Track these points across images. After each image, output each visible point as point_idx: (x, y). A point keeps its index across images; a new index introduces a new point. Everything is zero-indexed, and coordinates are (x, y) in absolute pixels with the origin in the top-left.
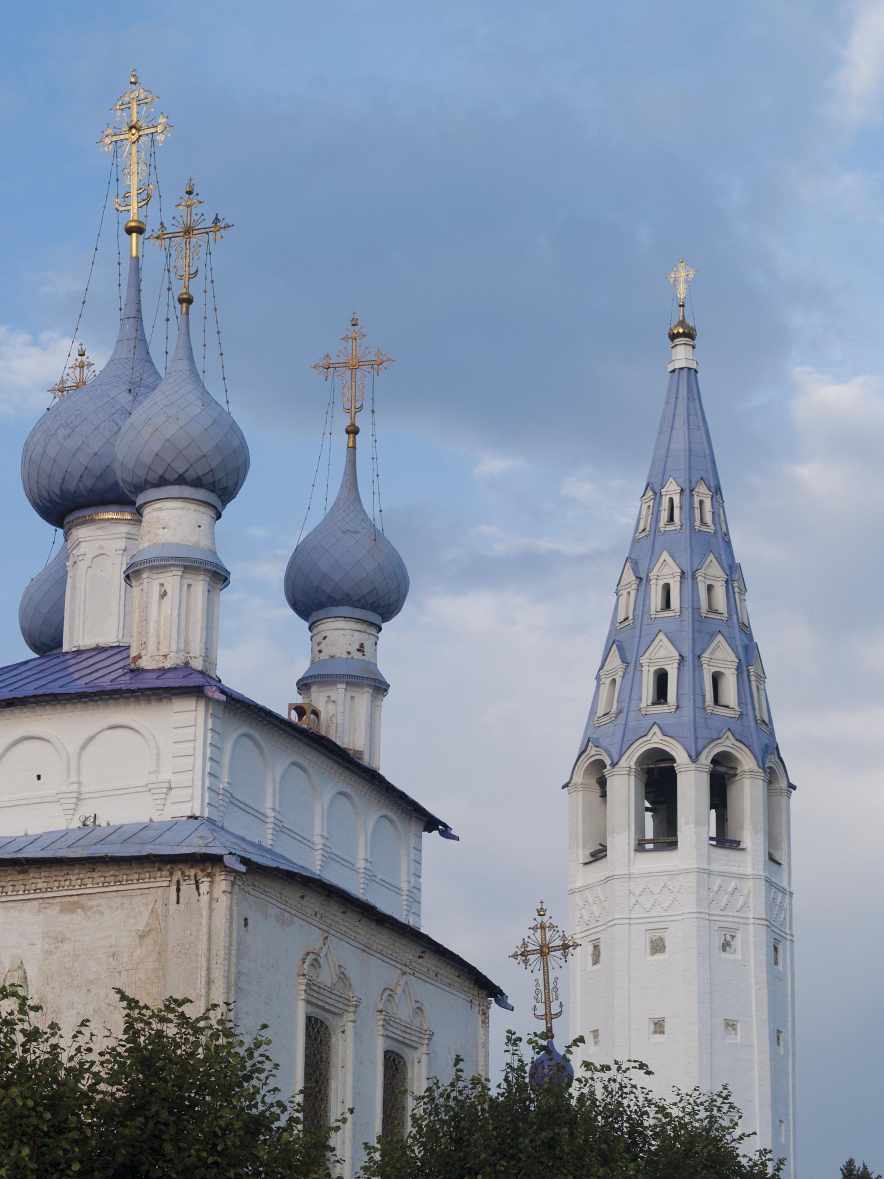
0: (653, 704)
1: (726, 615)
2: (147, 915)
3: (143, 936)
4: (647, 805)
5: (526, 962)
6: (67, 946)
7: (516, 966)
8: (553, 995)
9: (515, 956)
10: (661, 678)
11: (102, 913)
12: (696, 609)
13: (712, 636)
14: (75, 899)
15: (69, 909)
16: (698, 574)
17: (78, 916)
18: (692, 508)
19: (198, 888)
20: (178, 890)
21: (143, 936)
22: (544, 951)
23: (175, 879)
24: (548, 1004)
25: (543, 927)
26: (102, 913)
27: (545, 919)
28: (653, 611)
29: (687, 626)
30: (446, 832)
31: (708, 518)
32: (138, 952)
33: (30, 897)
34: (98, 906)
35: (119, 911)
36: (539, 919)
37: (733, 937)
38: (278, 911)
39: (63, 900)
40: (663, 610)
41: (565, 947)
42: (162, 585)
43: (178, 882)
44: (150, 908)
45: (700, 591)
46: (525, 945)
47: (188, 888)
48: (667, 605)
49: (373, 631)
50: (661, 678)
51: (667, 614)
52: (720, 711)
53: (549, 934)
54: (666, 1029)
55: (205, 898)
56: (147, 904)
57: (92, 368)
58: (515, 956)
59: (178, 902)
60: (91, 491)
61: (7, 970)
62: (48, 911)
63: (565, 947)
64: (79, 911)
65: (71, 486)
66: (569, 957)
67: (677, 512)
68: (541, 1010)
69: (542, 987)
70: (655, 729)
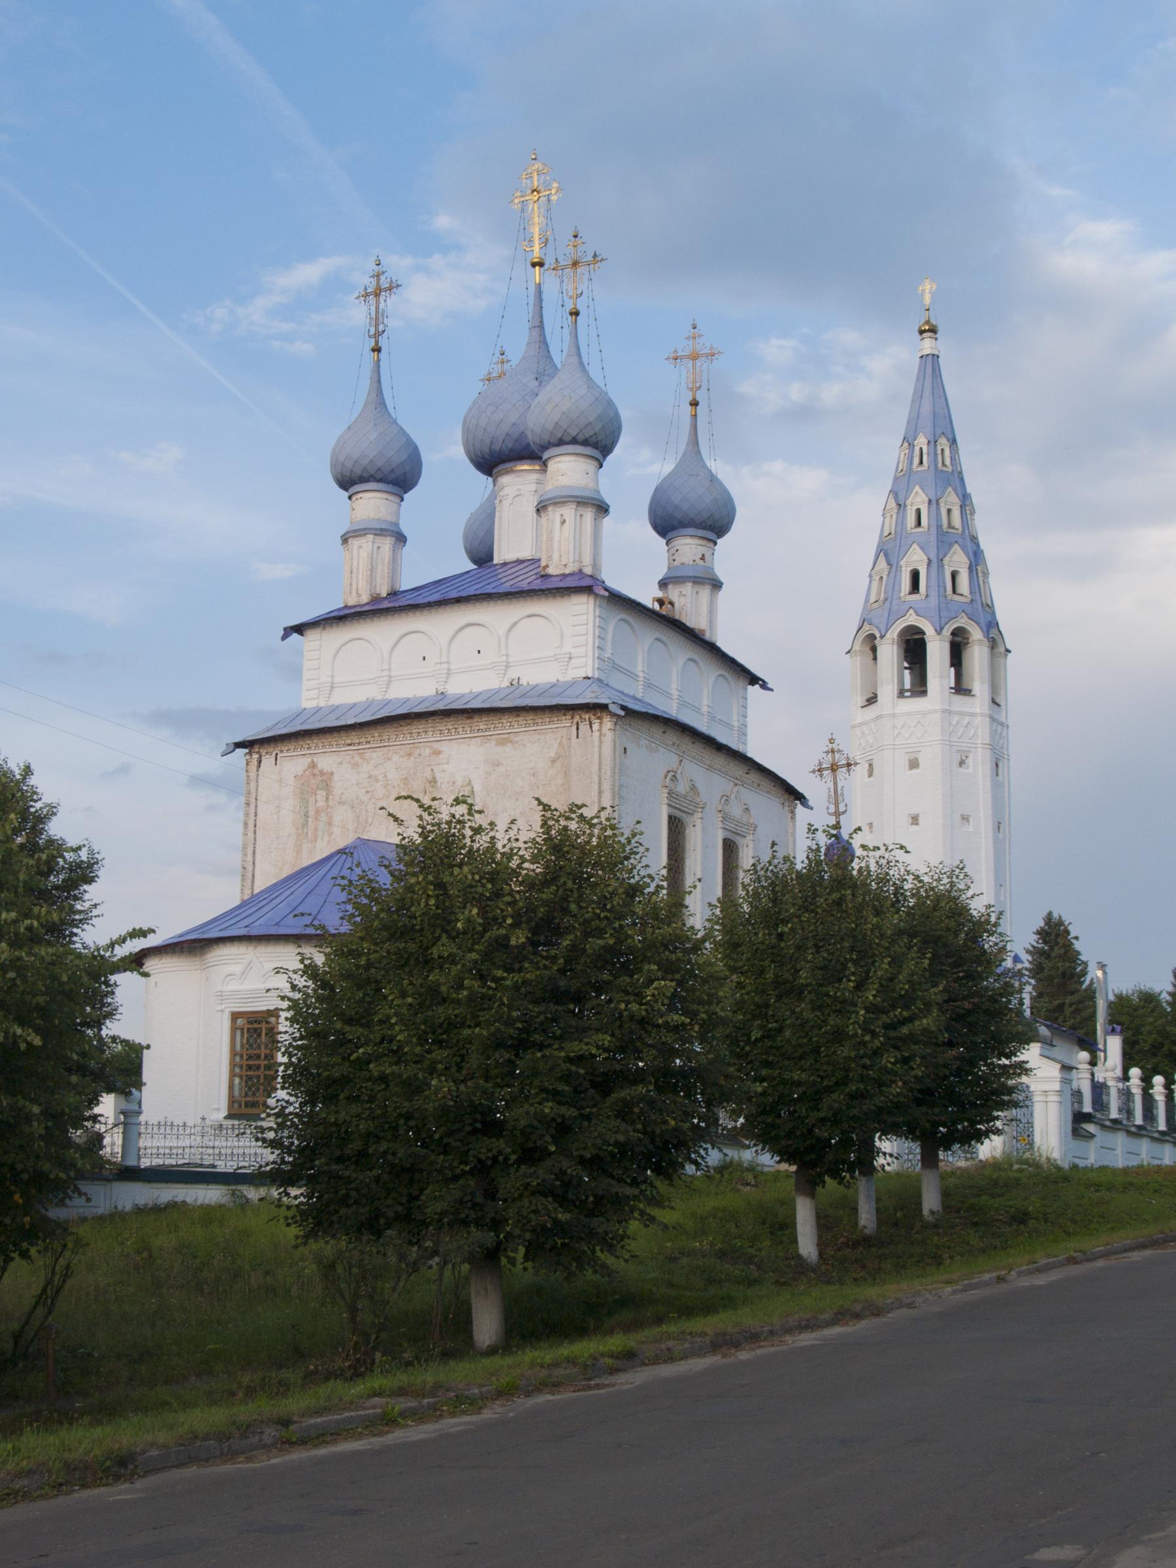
0: (910, 594)
1: (961, 530)
3: (553, 761)
4: (906, 665)
5: (821, 776)
6: (501, 769)
7: (815, 779)
8: (840, 799)
9: (813, 772)
10: (915, 576)
11: (525, 745)
12: (939, 526)
13: (951, 545)
15: (502, 743)
16: (941, 501)
18: (936, 454)
19: (591, 727)
20: (578, 729)
21: (553, 761)
22: (834, 768)
24: (837, 804)
25: (833, 751)
26: (525, 745)
28: (909, 528)
29: (933, 538)
30: (764, 686)
31: (948, 461)
37: (967, 757)
40: (916, 527)
41: (849, 765)
46: (820, 764)
47: (584, 727)
48: (919, 524)
49: (711, 545)
50: (915, 576)
51: (919, 530)
53: (837, 756)
55: (596, 734)
56: (556, 739)
58: (813, 772)
62: (487, 745)
63: (849, 765)
68: (832, 809)
69: (833, 794)
70: (911, 611)
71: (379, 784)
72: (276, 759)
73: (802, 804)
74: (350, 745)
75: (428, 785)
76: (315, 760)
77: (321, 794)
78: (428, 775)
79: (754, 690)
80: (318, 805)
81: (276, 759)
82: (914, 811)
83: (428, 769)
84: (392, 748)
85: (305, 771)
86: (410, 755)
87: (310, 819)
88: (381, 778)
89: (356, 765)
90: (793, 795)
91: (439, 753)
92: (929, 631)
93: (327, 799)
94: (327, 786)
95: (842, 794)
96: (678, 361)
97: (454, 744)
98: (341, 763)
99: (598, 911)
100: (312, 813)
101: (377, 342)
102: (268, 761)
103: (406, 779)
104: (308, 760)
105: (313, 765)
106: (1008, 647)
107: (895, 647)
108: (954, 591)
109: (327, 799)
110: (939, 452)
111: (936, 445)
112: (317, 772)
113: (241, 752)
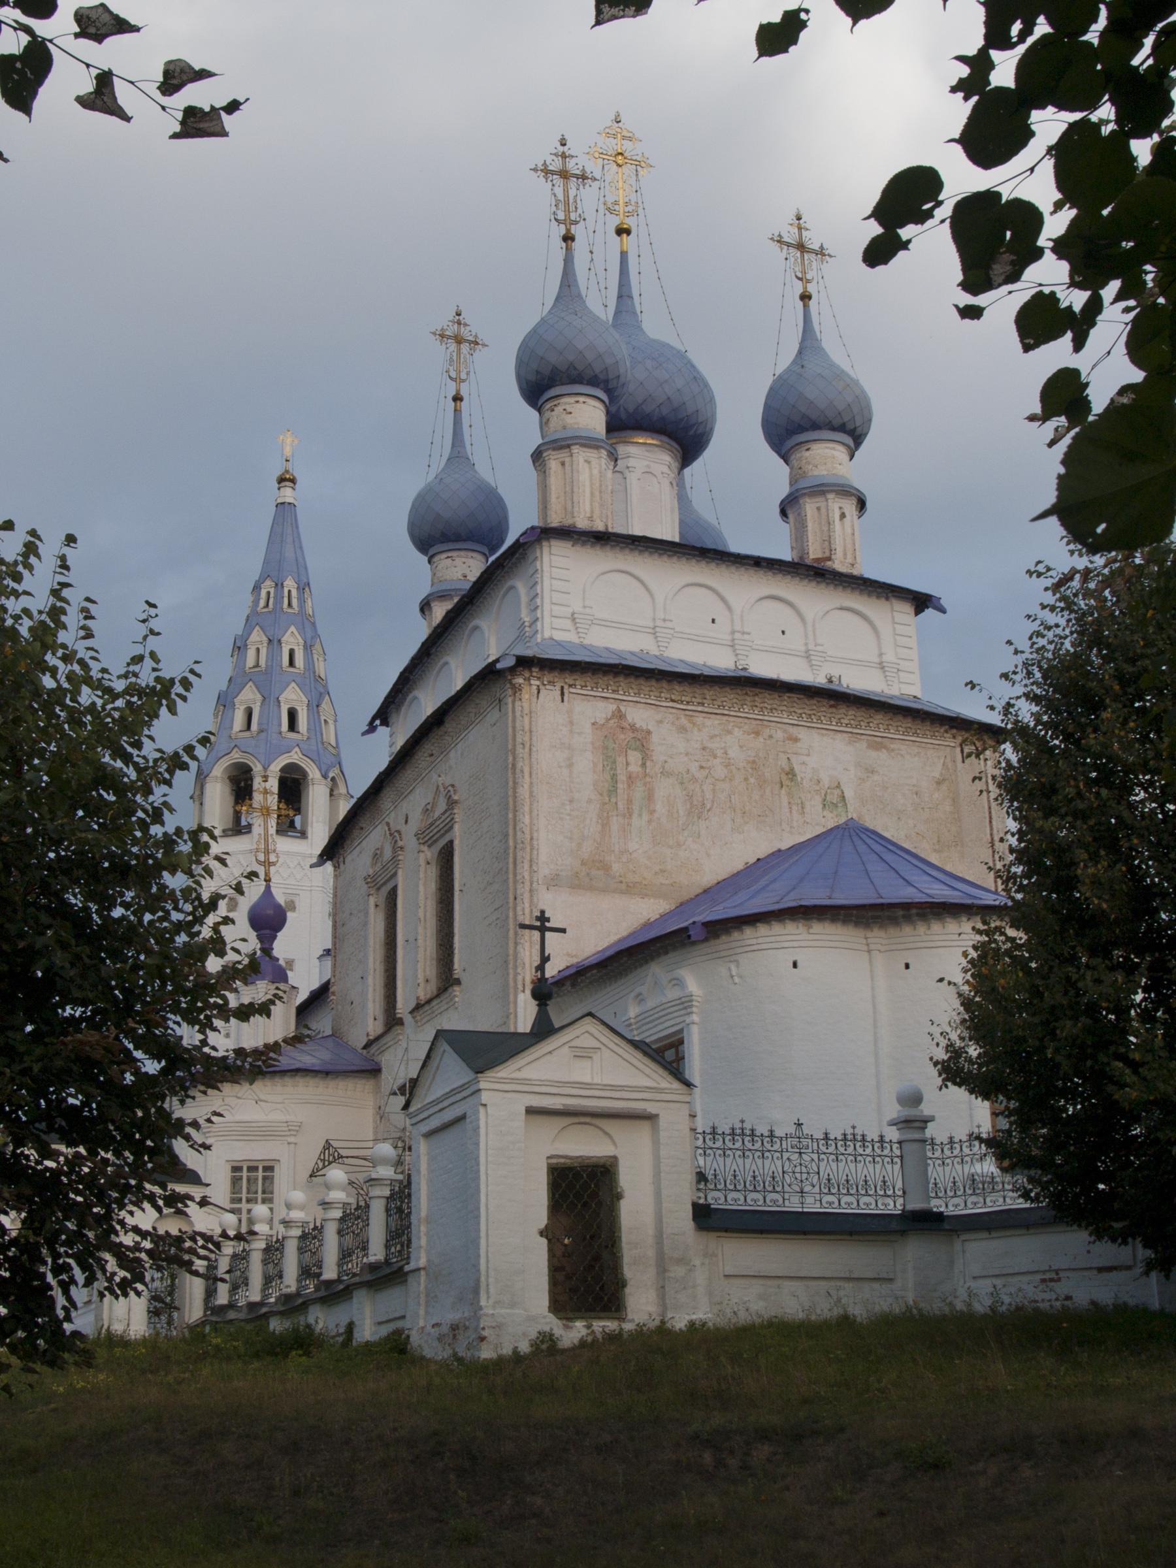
2: (940, 766)
3: (939, 783)
6: (876, 777)
14: (879, 739)
17: (883, 754)
31: (295, 602)
32: (936, 795)
33: (841, 729)
34: (899, 750)
35: (917, 758)
39: (870, 738)
42: (840, 508)
44: (942, 761)
45: (302, 657)
57: (468, 328)
60: (663, 419)
61: (827, 786)
62: (858, 745)
64: (883, 750)
65: (648, 408)
76: (623, 709)
83: (783, 757)
86: (757, 733)
87: (620, 785)
88: (719, 753)
89: (682, 729)
91: (796, 740)
98: (661, 722)
104: (612, 707)
112: (625, 725)
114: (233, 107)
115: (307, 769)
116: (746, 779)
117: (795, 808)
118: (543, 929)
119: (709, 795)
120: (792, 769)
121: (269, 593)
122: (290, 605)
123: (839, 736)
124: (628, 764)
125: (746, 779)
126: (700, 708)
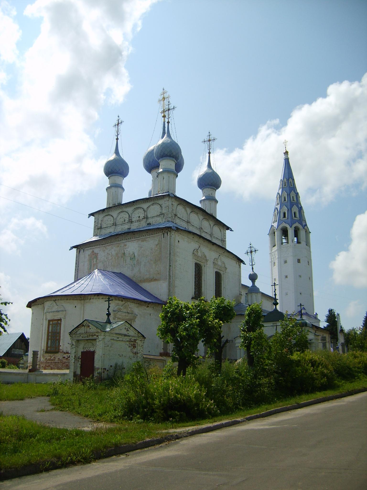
0: (283, 218)
1: (296, 201)
4: (283, 237)
5: (248, 254)
6: (142, 249)
7: (246, 255)
8: (253, 261)
9: (245, 253)
10: (284, 214)
11: (149, 241)
12: (290, 200)
13: (293, 205)
15: (143, 241)
16: (290, 194)
18: (289, 183)
19: (167, 234)
20: (164, 235)
21: (157, 245)
22: (251, 252)
23: (163, 233)
24: (252, 262)
25: (251, 247)
26: (149, 241)
27: (251, 246)
28: (282, 201)
29: (289, 204)
30: (231, 230)
31: (292, 184)
36: (250, 246)
38: (187, 240)
40: (284, 201)
41: (255, 251)
43: (164, 233)
46: (247, 251)
48: (285, 200)
49: (215, 190)
50: (284, 214)
51: (285, 202)
52: (296, 218)
53: (252, 248)
54: (288, 277)
55: (169, 236)
56: (158, 238)
58: (245, 253)
59: (164, 237)
62: (139, 242)
66: (256, 253)
67: (286, 183)
68: (251, 264)
69: (251, 259)
70: (284, 222)
71: (110, 256)
72: (84, 250)
73: (243, 263)
74: (102, 245)
75: (122, 255)
77: (95, 260)
78: (123, 252)
79: (228, 232)
80: (94, 263)
81: (84, 250)
82: (286, 275)
83: (123, 250)
84: (114, 245)
85: (91, 253)
86: (118, 247)
87: (92, 267)
88: (110, 254)
90: (240, 261)
91: (126, 245)
92: (288, 227)
93: (96, 261)
94: (96, 257)
95: (254, 259)
96: (205, 142)
97: (130, 243)
98: (100, 250)
99: (361, 362)
100: (92, 265)
101: (209, 151)
102: (82, 251)
103: (117, 253)
105: (93, 252)
106: (310, 231)
107: (280, 232)
108: (295, 217)
109: (96, 261)
110: (290, 182)
111: (289, 181)
112: (94, 253)
113: (75, 250)
114: (163, 90)
115: (201, 263)
116: (115, 258)
117: (124, 261)
118: (275, 285)
119: (107, 264)
120: (124, 253)
121: (285, 182)
122: (291, 185)
123: (135, 241)
124: (94, 262)
125: (115, 258)
126: (107, 245)
